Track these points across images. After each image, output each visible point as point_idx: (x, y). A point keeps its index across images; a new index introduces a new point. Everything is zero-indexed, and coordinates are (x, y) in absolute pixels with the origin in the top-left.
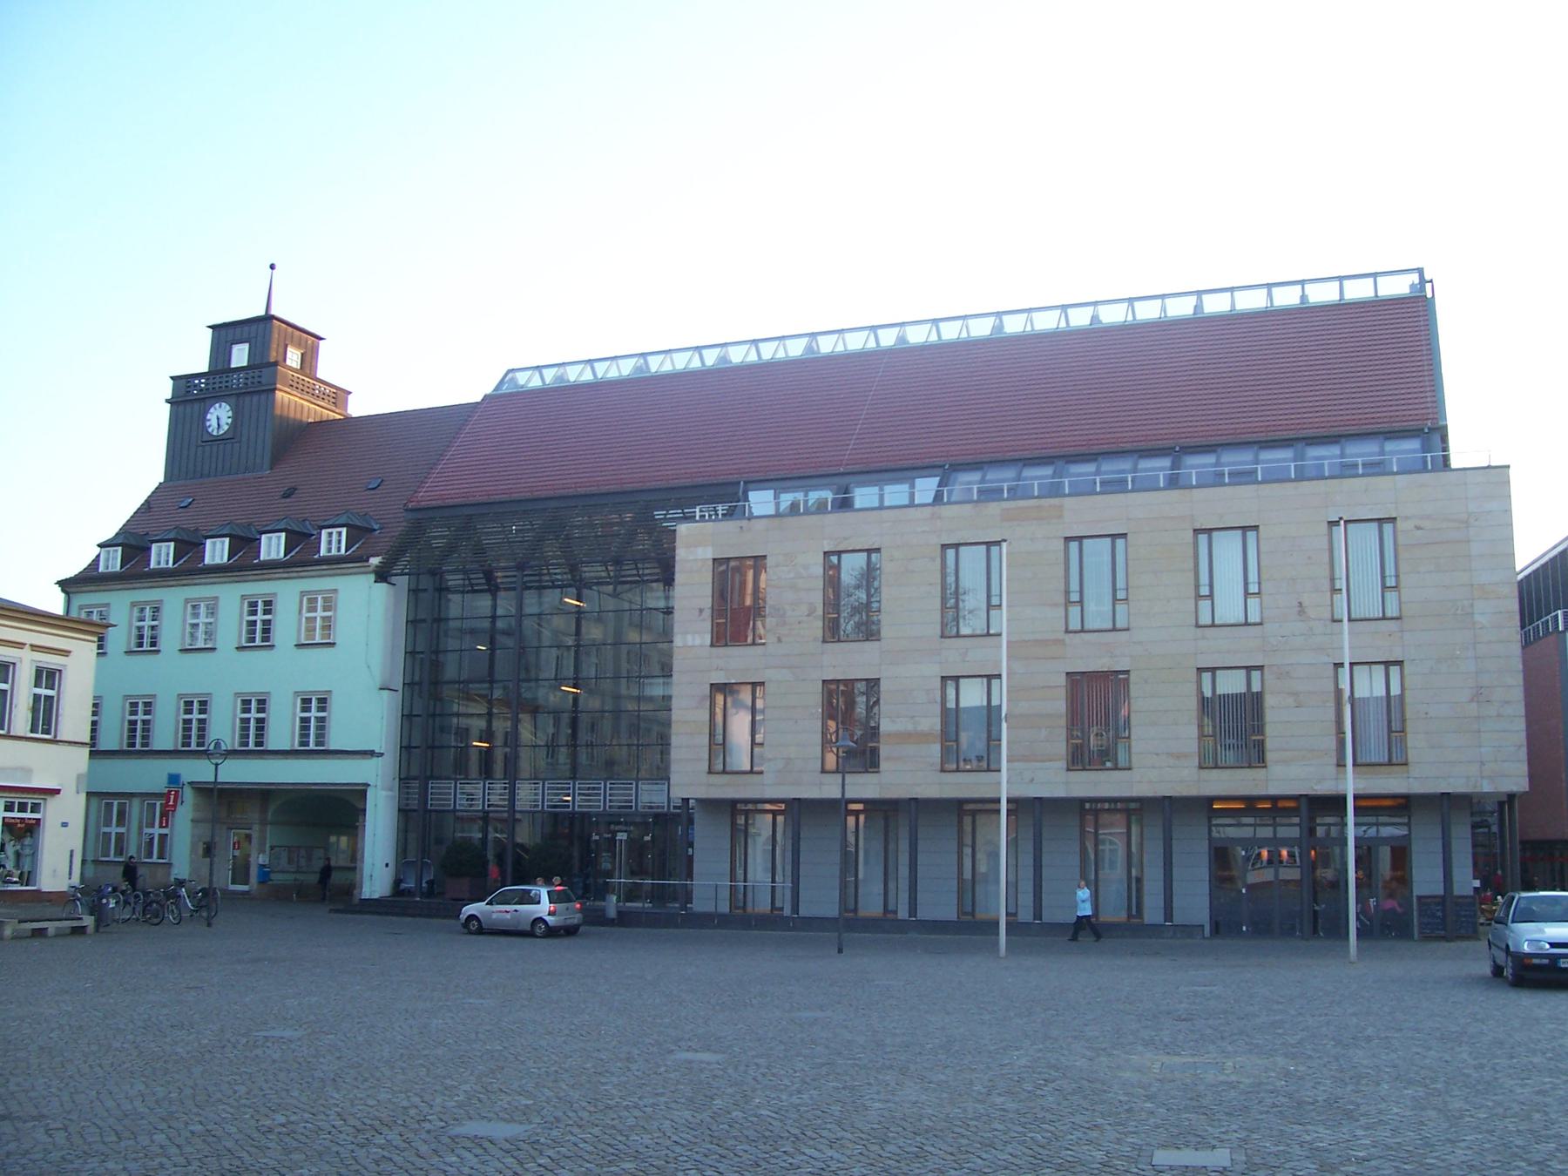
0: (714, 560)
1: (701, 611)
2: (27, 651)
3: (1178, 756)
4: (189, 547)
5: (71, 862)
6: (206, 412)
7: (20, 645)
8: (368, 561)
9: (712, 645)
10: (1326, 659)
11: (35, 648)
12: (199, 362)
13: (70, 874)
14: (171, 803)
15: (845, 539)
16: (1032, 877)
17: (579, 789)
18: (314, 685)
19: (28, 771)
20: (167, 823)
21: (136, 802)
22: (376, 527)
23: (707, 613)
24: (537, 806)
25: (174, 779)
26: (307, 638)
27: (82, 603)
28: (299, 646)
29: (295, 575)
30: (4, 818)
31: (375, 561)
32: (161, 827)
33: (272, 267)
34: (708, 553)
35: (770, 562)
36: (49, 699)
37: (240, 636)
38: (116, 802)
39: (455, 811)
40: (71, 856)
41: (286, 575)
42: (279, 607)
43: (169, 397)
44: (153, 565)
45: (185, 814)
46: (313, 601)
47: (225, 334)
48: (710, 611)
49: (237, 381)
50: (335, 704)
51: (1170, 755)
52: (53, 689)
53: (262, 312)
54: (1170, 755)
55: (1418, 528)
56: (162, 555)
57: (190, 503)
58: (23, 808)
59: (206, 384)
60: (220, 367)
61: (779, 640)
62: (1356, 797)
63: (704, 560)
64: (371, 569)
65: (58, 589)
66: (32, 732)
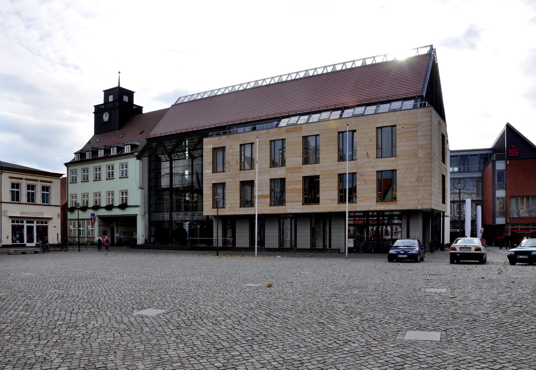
0: (213, 148)
1: (210, 163)
2: (39, 182)
3: (332, 200)
4: (107, 151)
6: (103, 115)
7: (37, 181)
8: (134, 154)
10: (374, 170)
11: (26, 179)
12: (101, 101)
13: (58, 239)
16: (265, 237)
17: (198, 215)
18: (124, 188)
19: (42, 213)
21: (86, 221)
22: (139, 144)
24: (202, 219)
25: (93, 215)
26: (122, 176)
27: (83, 167)
28: (120, 178)
29: (118, 159)
31: (136, 154)
33: (119, 72)
34: (211, 147)
35: (226, 148)
37: (107, 176)
38: (72, 222)
39: (175, 221)
40: (58, 235)
42: (115, 168)
43: (94, 111)
44: (99, 156)
46: (123, 165)
47: (107, 93)
49: (111, 105)
50: (129, 193)
51: (330, 200)
53: (117, 86)
54: (330, 200)
55: (402, 128)
56: (101, 153)
58: (42, 223)
59: (104, 107)
60: (115, 100)
61: (229, 170)
62: (349, 212)
63: (211, 148)
65: (499, 130)
66: (42, 203)
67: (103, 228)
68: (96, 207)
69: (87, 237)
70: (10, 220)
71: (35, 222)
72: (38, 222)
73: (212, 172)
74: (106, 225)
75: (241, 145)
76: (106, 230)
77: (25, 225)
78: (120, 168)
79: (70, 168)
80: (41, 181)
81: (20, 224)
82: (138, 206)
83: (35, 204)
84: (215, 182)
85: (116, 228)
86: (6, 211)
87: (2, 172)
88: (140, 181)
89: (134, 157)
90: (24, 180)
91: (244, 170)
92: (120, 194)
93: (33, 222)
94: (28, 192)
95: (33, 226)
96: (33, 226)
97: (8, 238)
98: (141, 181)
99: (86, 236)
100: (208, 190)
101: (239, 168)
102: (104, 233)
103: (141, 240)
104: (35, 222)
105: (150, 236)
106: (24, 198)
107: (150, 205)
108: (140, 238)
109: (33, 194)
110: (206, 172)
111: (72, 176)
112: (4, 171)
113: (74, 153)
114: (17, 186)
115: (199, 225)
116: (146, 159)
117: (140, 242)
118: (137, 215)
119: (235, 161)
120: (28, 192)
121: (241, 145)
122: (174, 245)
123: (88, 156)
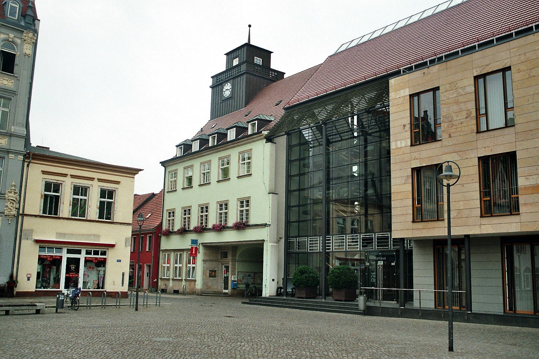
1: (404, 126)
5: (123, 278)
9: (412, 145)
11: (73, 176)
13: (123, 284)
14: (194, 253)
15: (487, 65)
19: (98, 236)
20: (195, 262)
21: (185, 253)
23: (408, 127)
25: (194, 242)
29: (236, 145)
30: (85, 257)
31: (265, 133)
32: (193, 264)
33: (250, 26)
34: (407, 92)
36: (85, 200)
39: (333, 252)
40: (123, 275)
41: (232, 146)
45: (200, 257)
47: (230, 55)
48: (409, 125)
50: (252, 203)
52: (113, 199)
57: (215, 126)
58: (96, 253)
64: (262, 137)
66: (99, 218)
67: (212, 266)
68: (201, 230)
69: (186, 280)
70: (37, 247)
71: (84, 252)
72: (88, 253)
73: (409, 144)
74: (217, 261)
75: (476, 78)
76: (216, 269)
77: (65, 256)
78: (239, 159)
79: (170, 169)
80: (100, 180)
81: (99, 256)
82: (265, 225)
83: (86, 220)
84: (417, 164)
85: (232, 265)
86: (32, 231)
87: (30, 162)
88: (270, 181)
89: (261, 139)
90: (69, 177)
91: (488, 130)
92: (237, 204)
93: (79, 252)
94: (74, 199)
95: (79, 259)
96: (79, 259)
97: (29, 279)
98: (274, 177)
99: (184, 278)
100: (403, 182)
101: (474, 128)
102: (213, 274)
103: (268, 289)
104: (84, 252)
105: (286, 280)
106: (65, 209)
107: (288, 223)
108: (268, 284)
109: (84, 203)
110: (396, 145)
111: (171, 180)
112: (32, 161)
113: (176, 146)
114: (57, 187)
115: (380, 260)
116: (282, 141)
117: (268, 292)
118: (264, 240)
119: (464, 114)
120: (74, 199)
121: (476, 78)
122: (330, 300)
123: (196, 147)
